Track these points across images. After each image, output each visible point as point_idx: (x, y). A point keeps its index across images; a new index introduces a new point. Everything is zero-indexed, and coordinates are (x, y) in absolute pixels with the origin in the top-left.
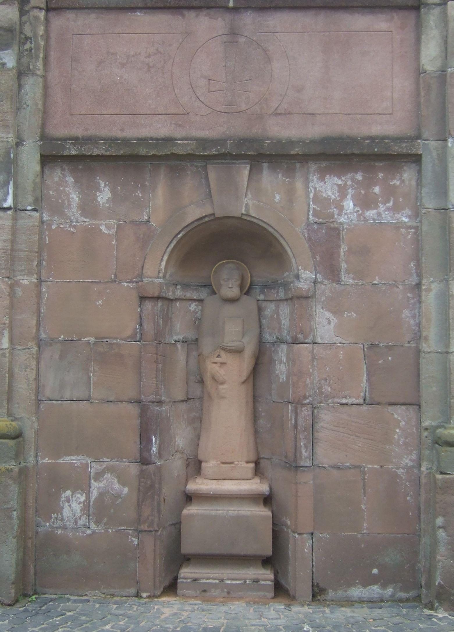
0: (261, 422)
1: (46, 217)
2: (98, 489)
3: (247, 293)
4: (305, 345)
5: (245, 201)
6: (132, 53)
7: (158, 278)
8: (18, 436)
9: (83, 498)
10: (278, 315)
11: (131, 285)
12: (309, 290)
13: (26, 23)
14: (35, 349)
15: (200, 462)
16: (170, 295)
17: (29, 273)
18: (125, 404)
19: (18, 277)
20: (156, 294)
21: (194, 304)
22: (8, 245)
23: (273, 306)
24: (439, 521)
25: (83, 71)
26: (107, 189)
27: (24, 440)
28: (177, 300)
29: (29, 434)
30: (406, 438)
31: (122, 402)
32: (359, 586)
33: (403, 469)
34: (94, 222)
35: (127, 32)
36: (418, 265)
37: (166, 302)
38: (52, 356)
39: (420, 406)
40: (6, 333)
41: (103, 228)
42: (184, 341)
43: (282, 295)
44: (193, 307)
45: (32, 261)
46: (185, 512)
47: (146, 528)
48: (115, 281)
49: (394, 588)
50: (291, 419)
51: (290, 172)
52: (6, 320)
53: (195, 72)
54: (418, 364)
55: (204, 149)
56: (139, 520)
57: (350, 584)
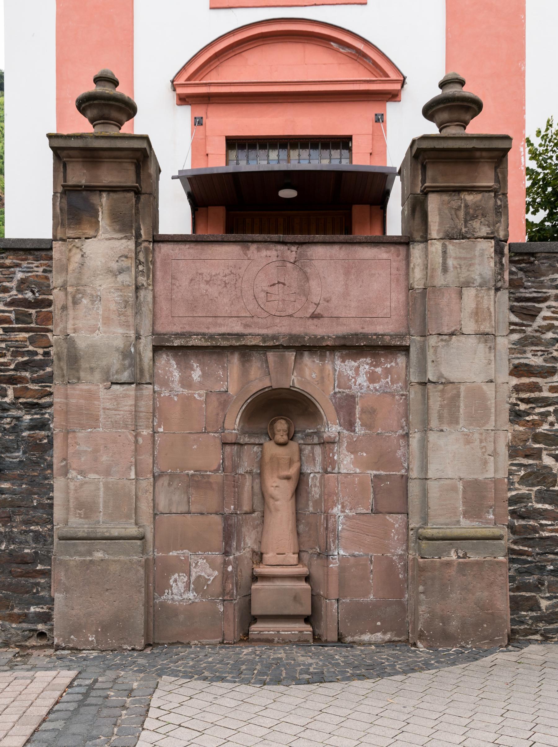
0: (301, 527)
1: (157, 388)
2: (196, 573)
3: (292, 439)
4: (333, 475)
5: (293, 377)
6: (214, 274)
7: (234, 429)
8: (142, 538)
9: (186, 579)
10: (313, 454)
11: (216, 435)
12: (335, 437)
13: (139, 252)
14: (152, 479)
15: (262, 554)
16: (241, 441)
17: (147, 427)
18: (213, 516)
19: (140, 430)
20: (233, 441)
21: (256, 447)
22: (133, 408)
23: (309, 447)
24: (421, 588)
25: (180, 286)
26: (198, 369)
27: (146, 541)
28: (246, 444)
29: (149, 536)
30: (399, 536)
31: (211, 514)
32: (369, 633)
33: (397, 556)
34: (190, 392)
35: (210, 258)
36: (407, 420)
37: (239, 446)
38: (163, 484)
39: (408, 514)
40: (133, 468)
41: (196, 396)
42: (250, 473)
43: (316, 440)
44: (256, 448)
45: (149, 419)
46: (253, 587)
47: (229, 598)
48: (205, 432)
49: (391, 635)
50: (323, 524)
51: (322, 358)
52: (133, 460)
53: (257, 287)
54: (407, 486)
55: (265, 342)
56: (224, 592)
57: (363, 633)
